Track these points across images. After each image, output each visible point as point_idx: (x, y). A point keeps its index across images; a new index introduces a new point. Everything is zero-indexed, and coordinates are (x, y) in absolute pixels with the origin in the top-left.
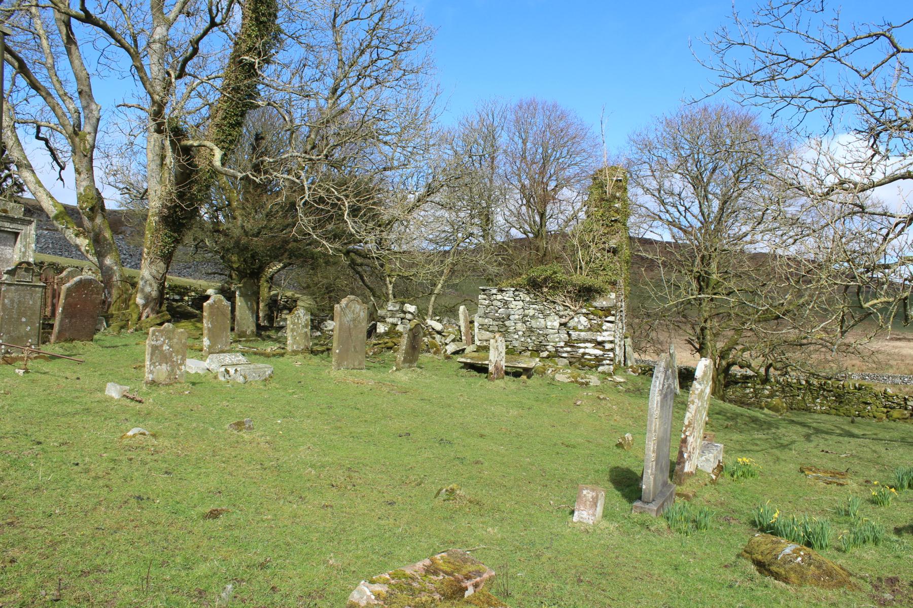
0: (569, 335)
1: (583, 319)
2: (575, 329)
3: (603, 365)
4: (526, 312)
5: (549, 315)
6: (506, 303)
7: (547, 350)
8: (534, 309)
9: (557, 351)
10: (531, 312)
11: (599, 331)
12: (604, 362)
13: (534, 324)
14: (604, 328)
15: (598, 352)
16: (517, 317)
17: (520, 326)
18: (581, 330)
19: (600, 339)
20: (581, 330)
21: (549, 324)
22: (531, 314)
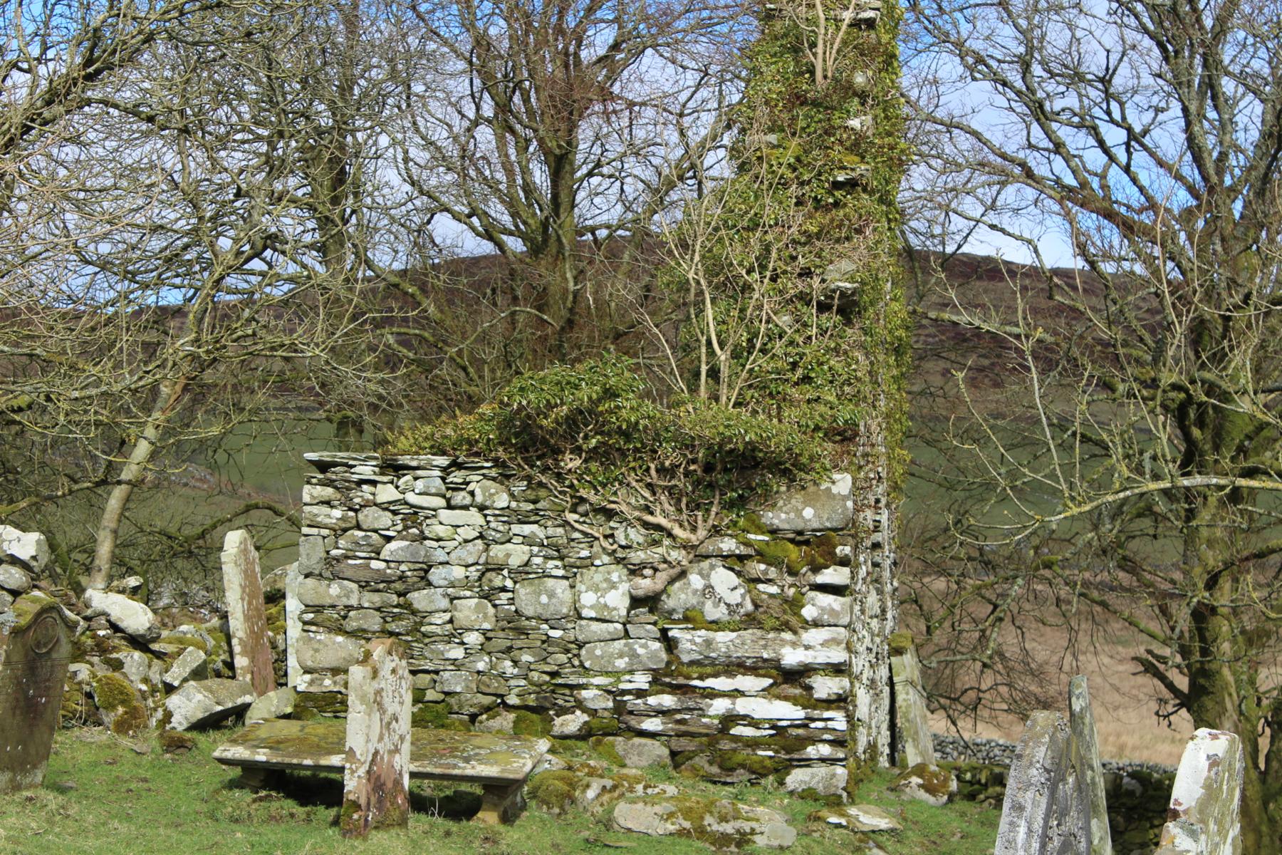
0: (670, 644)
1: (723, 579)
2: (691, 619)
3: (806, 763)
4: (497, 551)
5: (588, 563)
6: (413, 517)
7: (580, 705)
8: (528, 540)
9: (620, 709)
10: (517, 554)
11: (786, 626)
12: (811, 751)
13: (528, 599)
14: (808, 612)
15: (786, 711)
16: (458, 572)
17: (469, 609)
18: (715, 625)
19: (792, 657)
20: (715, 625)
21: (588, 599)
22: (515, 562)
